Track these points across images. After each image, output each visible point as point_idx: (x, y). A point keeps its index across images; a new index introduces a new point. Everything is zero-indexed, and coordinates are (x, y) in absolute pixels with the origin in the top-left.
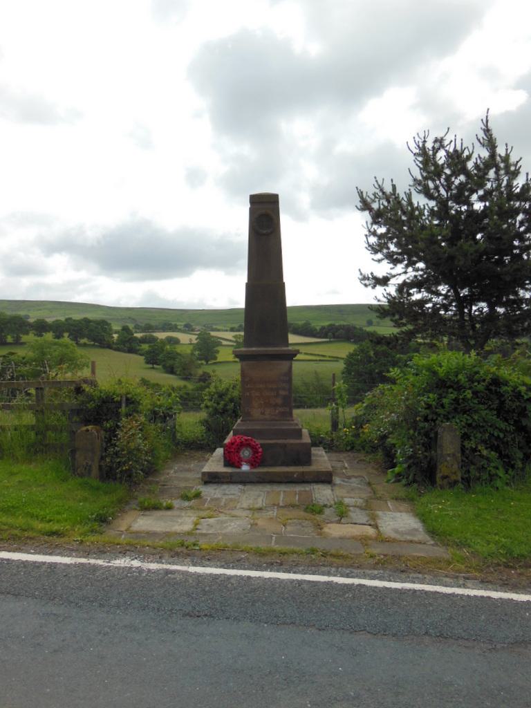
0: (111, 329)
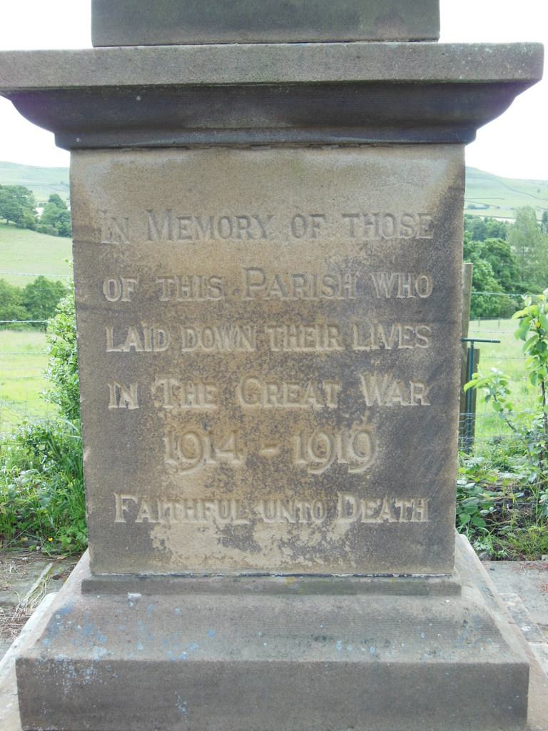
0: (32, 201)
